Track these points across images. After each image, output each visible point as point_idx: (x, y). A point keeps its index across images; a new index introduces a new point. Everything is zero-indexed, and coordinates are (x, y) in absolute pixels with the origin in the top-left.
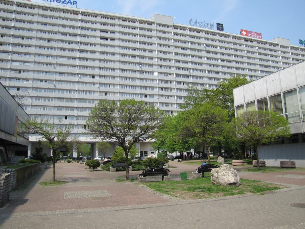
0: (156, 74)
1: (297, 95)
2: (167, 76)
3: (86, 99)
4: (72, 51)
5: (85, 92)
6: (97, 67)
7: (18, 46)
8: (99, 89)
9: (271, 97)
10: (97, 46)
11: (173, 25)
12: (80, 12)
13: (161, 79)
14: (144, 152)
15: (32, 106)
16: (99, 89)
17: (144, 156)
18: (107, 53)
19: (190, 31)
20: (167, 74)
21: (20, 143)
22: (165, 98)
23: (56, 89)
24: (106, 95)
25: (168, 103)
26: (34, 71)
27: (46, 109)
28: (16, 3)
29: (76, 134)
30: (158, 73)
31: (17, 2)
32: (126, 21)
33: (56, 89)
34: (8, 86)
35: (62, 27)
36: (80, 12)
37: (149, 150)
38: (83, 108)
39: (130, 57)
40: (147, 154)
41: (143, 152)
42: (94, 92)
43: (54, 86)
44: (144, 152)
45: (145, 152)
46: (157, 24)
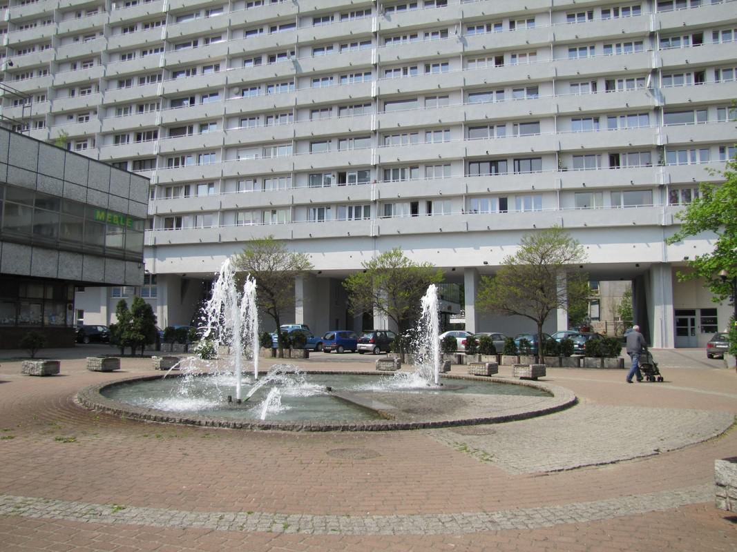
1: (258, 369)
4: (720, 35)
5: (408, 66)
7: (673, 78)
8: (465, 45)
9: (716, 318)
14: (698, 313)
15: (227, 148)
16: (465, 45)
17: (698, 330)
21: (119, 261)
23: (301, 77)
24: (607, 88)
26: (233, 30)
27: (272, 153)
29: (664, 227)
33: (301, 77)
40: (715, 321)
41: (692, 312)
42: (443, 61)
43: (292, 66)
44: (698, 313)
45: (704, 312)
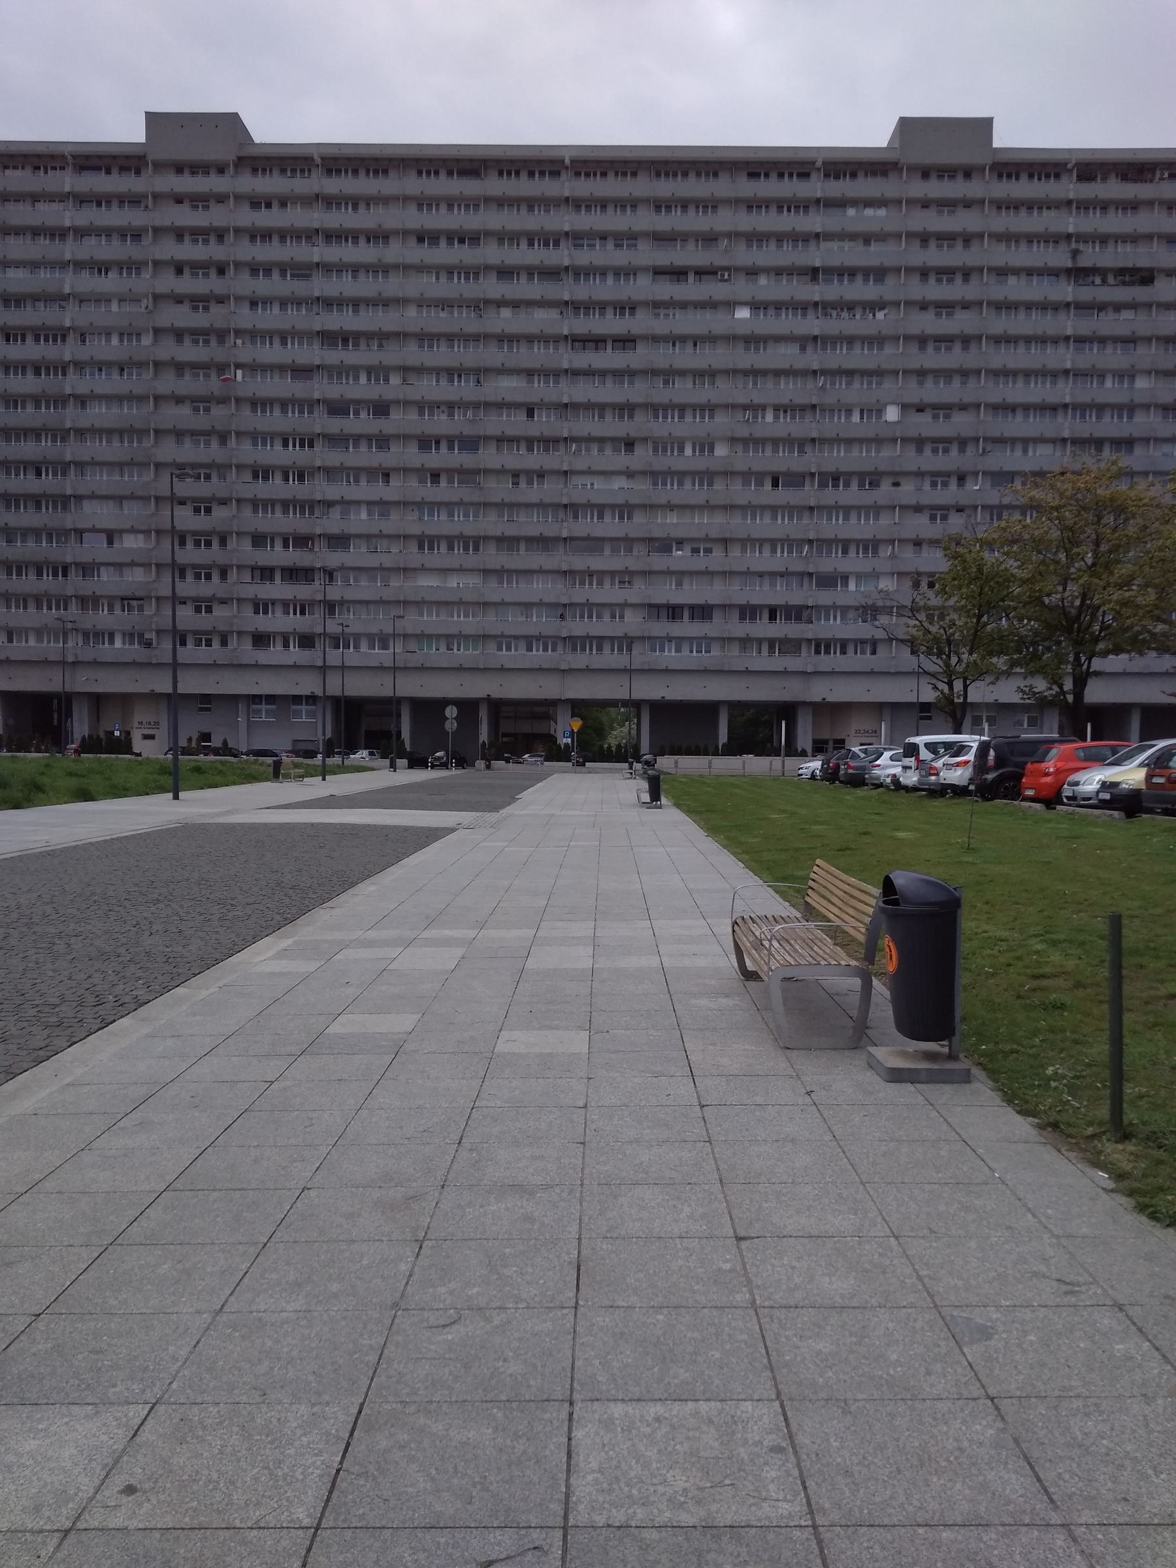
0: (892, 414)
2: (949, 315)
3: (602, 540)
6: (645, 269)
10: (641, 314)
11: (990, 162)
12: (567, 161)
13: (917, 332)
18: (684, 204)
19: (1082, 178)
20: (952, 341)
22: (939, 315)
25: (948, 441)
28: (319, 161)
30: (905, 407)
31: (322, 159)
32: (767, 175)
34: (319, 501)
35: (499, 205)
36: (567, 161)
37: (853, 733)
38: (589, 638)
39: (785, 209)
44: (831, 743)
46: (912, 169)
